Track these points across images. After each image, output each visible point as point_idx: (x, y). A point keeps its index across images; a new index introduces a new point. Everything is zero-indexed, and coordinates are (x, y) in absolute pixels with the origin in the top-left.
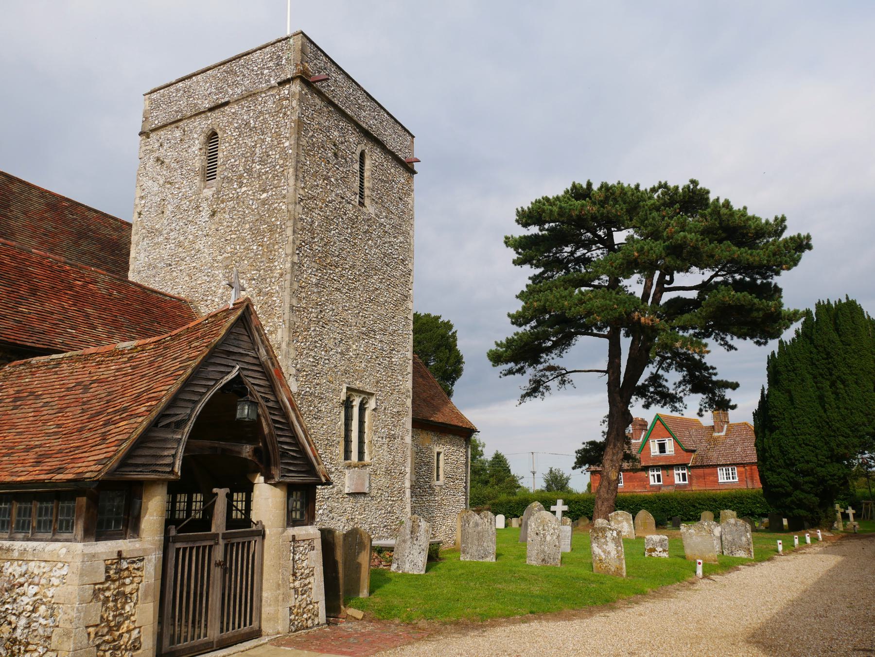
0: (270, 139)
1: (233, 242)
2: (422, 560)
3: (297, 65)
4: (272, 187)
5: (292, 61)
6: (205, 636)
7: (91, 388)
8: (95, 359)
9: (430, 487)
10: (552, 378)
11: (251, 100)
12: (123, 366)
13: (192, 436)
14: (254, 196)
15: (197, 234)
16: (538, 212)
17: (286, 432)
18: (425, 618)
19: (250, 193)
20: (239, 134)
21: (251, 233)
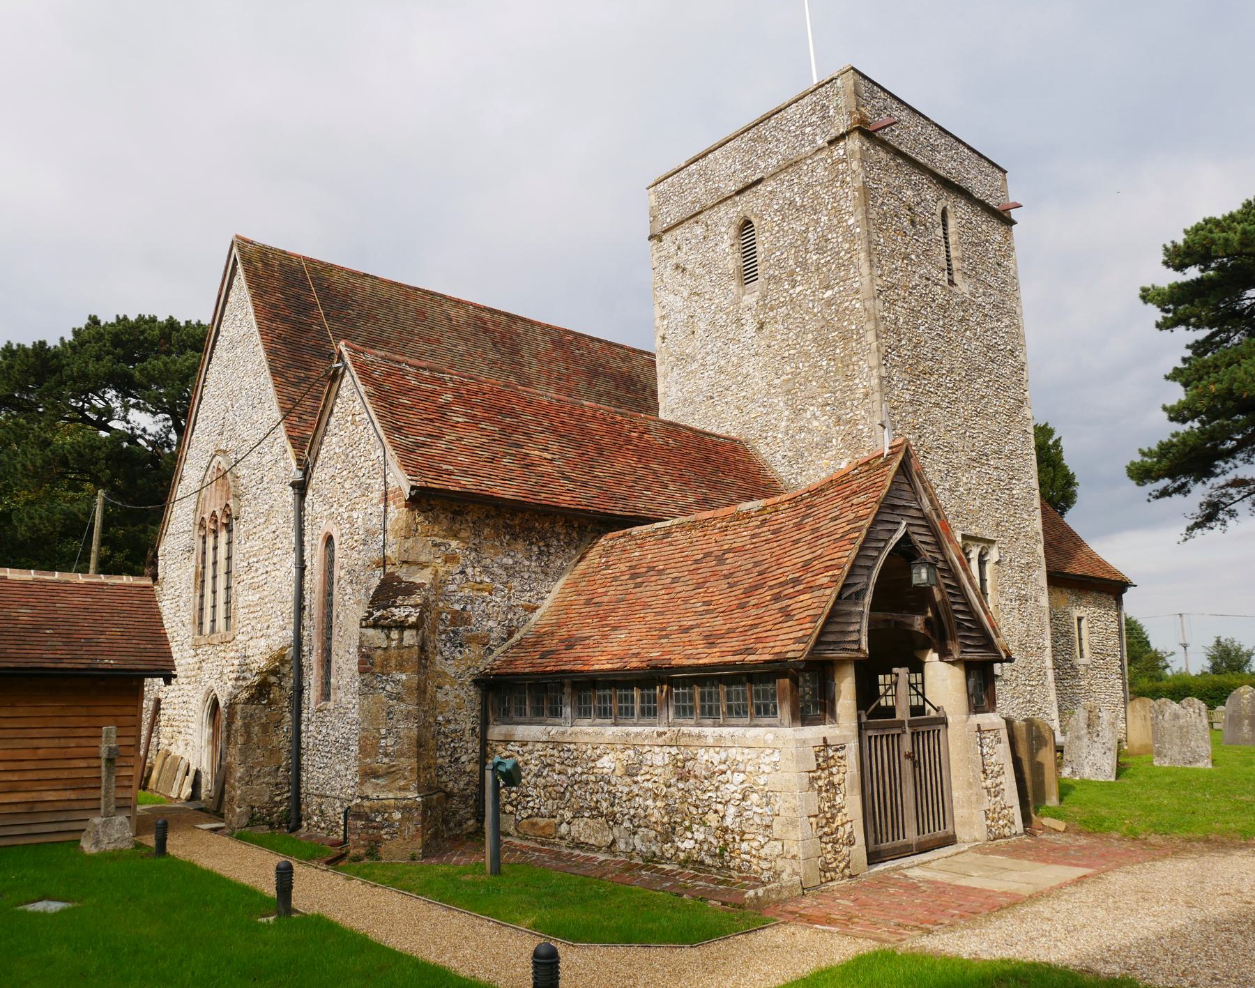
2: (1108, 765)
3: (851, 113)
5: (844, 109)
8: (715, 525)
9: (1072, 667)
10: (1240, 497)
12: (757, 531)
13: (873, 608)
16: (1204, 245)
18: (1156, 832)
19: (808, 292)
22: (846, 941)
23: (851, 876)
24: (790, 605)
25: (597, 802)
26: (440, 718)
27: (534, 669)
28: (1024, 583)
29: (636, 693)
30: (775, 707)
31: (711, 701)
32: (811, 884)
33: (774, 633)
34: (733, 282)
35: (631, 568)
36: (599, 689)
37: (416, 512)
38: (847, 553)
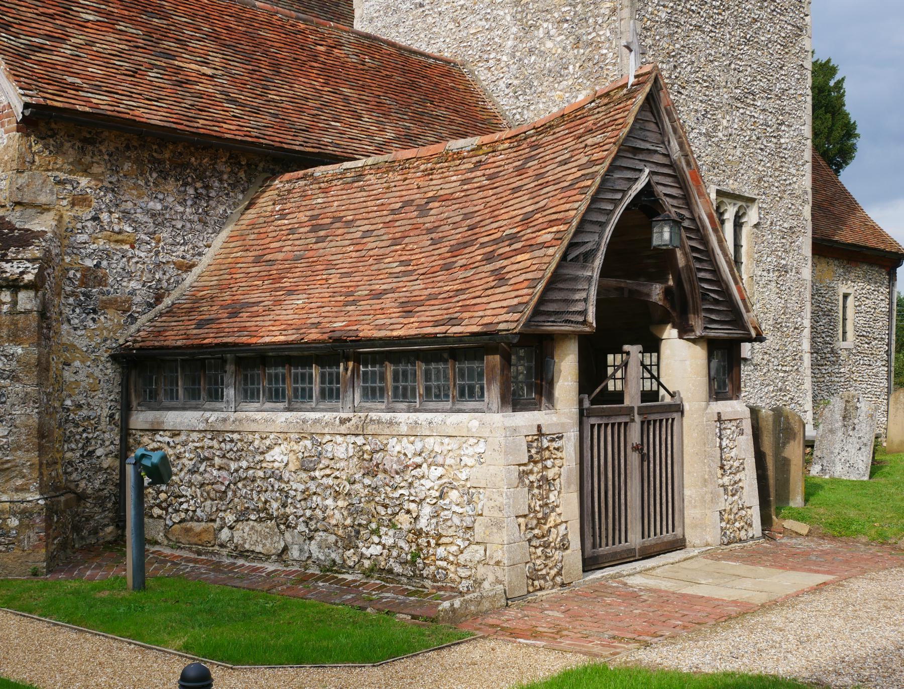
2: (862, 461)
6: (626, 541)
7: (431, 209)
8: (418, 167)
9: (832, 351)
12: (469, 175)
13: (604, 273)
17: (704, 264)
22: (552, 656)
23: (563, 585)
24: (504, 267)
25: (266, 502)
26: (68, 402)
27: (189, 342)
28: (785, 251)
29: (315, 371)
30: (482, 388)
31: (406, 381)
32: (517, 594)
33: (484, 300)
35: (313, 218)
36: (270, 367)
37: (32, 138)
38: (576, 205)
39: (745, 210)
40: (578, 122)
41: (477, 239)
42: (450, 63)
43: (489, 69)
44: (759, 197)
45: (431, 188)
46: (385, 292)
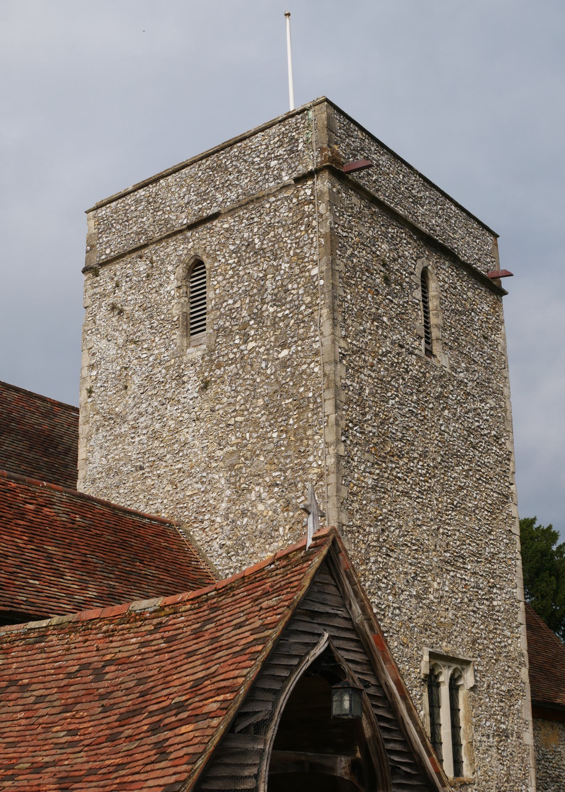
0: (288, 265)
1: (240, 428)
3: (322, 150)
4: (296, 339)
5: (314, 144)
7: (107, 673)
8: (100, 628)
11: (253, 209)
12: (149, 637)
13: (278, 744)
14: (268, 354)
15: (181, 419)
17: (394, 734)
19: (262, 350)
20: (238, 261)
21: (267, 413)
24: (167, 740)
28: (505, 715)
34: (176, 331)
38: (245, 672)
39: (461, 672)
40: (257, 584)
41: (146, 707)
42: (165, 523)
43: (204, 529)
44: (474, 659)
45: (110, 650)
46: (47, 765)
